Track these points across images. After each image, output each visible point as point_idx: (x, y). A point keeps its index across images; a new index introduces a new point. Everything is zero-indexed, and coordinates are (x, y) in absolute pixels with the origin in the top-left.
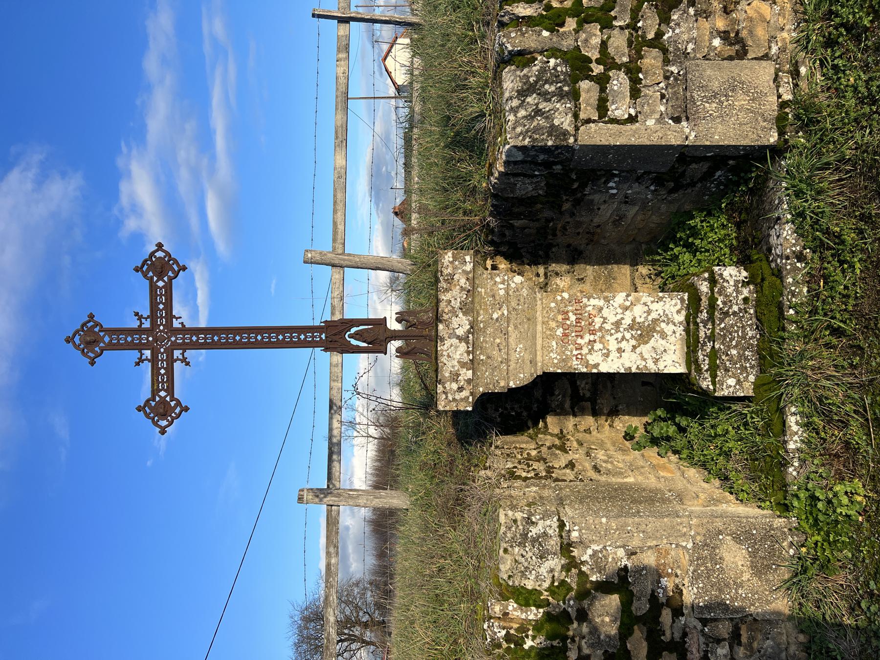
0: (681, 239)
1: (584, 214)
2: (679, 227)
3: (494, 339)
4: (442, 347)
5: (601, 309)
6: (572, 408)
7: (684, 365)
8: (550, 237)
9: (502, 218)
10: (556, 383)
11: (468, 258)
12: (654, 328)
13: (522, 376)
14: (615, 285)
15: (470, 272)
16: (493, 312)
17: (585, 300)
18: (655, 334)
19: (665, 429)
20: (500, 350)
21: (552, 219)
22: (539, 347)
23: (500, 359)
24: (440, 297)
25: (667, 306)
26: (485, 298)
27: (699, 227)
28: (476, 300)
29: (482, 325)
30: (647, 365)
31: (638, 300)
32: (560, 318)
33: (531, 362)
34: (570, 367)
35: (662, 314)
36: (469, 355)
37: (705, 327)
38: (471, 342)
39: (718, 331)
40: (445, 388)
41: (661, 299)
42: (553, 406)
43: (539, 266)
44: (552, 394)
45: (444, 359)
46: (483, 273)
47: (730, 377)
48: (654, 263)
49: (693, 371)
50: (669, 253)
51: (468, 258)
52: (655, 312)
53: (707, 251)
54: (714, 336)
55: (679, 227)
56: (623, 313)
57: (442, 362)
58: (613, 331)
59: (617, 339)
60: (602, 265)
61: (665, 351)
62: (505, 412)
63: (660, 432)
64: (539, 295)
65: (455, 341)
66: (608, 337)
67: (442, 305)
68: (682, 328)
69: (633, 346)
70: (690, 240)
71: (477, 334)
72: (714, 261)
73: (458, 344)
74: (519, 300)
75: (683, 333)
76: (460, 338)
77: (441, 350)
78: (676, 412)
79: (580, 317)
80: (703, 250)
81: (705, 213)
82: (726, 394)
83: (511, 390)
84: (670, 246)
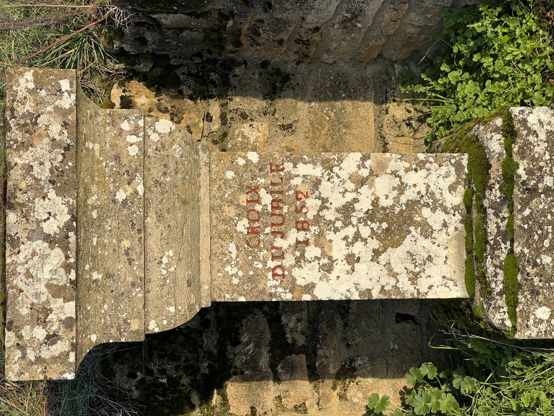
0: (460, 55)
1: (288, 5)
2: (457, 34)
3: (120, 241)
4: (14, 258)
5: (317, 183)
6: (273, 366)
7: (461, 283)
8: (230, 47)
9: (136, 7)
10: (244, 321)
11: (65, 85)
12: (411, 218)
13: (172, 309)
14: (349, 139)
15: (70, 110)
16: (117, 188)
17: (288, 166)
18: (412, 228)
19: (434, 400)
20: (130, 261)
21: (232, 14)
22: (204, 255)
23: (130, 279)
24: (10, 158)
25: (433, 177)
26: (99, 162)
27: (489, 34)
28: (84, 166)
29: (95, 214)
30: (400, 285)
31: (382, 166)
32: (243, 199)
33: (189, 284)
34: (263, 291)
35: (423, 192)
36: (68, 272)
37: (496, 215)
38: (72, 246)
39: (519, 222)
40: (20, 337)
41: (421, 165)
42: (238, 364)
43: (211, 101)
44: (236, 342)
45: (18, 281)
46: (96, 114)
47: (541, 304)
48: (414, 98)
49: (478, 294)
50: (440, 81)
51: (65, 85)
52: (413, 189)
53: (504, 78)
54: (512, 231)
55: (457, 34)
56: (356, 191)
57: (15, 287)
58: (339, 224)
59: (346, 238)
60: (325, 100)
61: (430, 258)
62: (148, 378)
63: (426, 406)
64: (203, 157)
65: (40, 245)
66: (330, 235)
67: (15, 175)
68: (458, 217)
69: (374, 251)
70: (476, 58)
71: (86, 231)
72: (515, 96)
73: (48, 251)
74: (165, 166)
75: (460, 226)
76: (50, 240)
77: (12, 263)
78: (455, 368)
79: (280, 197)
80: (497, 76)
81: (499, 9)
82: (534, 335)
83: (151, 337)
84: (442, 68)
